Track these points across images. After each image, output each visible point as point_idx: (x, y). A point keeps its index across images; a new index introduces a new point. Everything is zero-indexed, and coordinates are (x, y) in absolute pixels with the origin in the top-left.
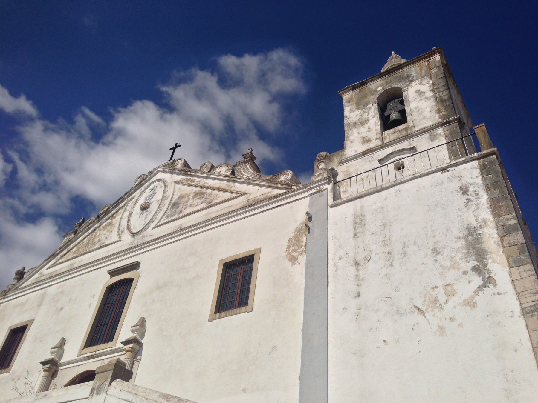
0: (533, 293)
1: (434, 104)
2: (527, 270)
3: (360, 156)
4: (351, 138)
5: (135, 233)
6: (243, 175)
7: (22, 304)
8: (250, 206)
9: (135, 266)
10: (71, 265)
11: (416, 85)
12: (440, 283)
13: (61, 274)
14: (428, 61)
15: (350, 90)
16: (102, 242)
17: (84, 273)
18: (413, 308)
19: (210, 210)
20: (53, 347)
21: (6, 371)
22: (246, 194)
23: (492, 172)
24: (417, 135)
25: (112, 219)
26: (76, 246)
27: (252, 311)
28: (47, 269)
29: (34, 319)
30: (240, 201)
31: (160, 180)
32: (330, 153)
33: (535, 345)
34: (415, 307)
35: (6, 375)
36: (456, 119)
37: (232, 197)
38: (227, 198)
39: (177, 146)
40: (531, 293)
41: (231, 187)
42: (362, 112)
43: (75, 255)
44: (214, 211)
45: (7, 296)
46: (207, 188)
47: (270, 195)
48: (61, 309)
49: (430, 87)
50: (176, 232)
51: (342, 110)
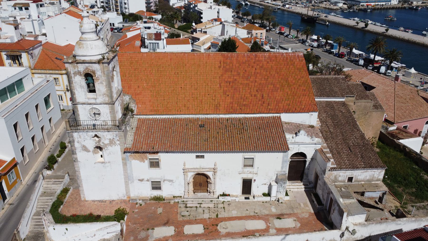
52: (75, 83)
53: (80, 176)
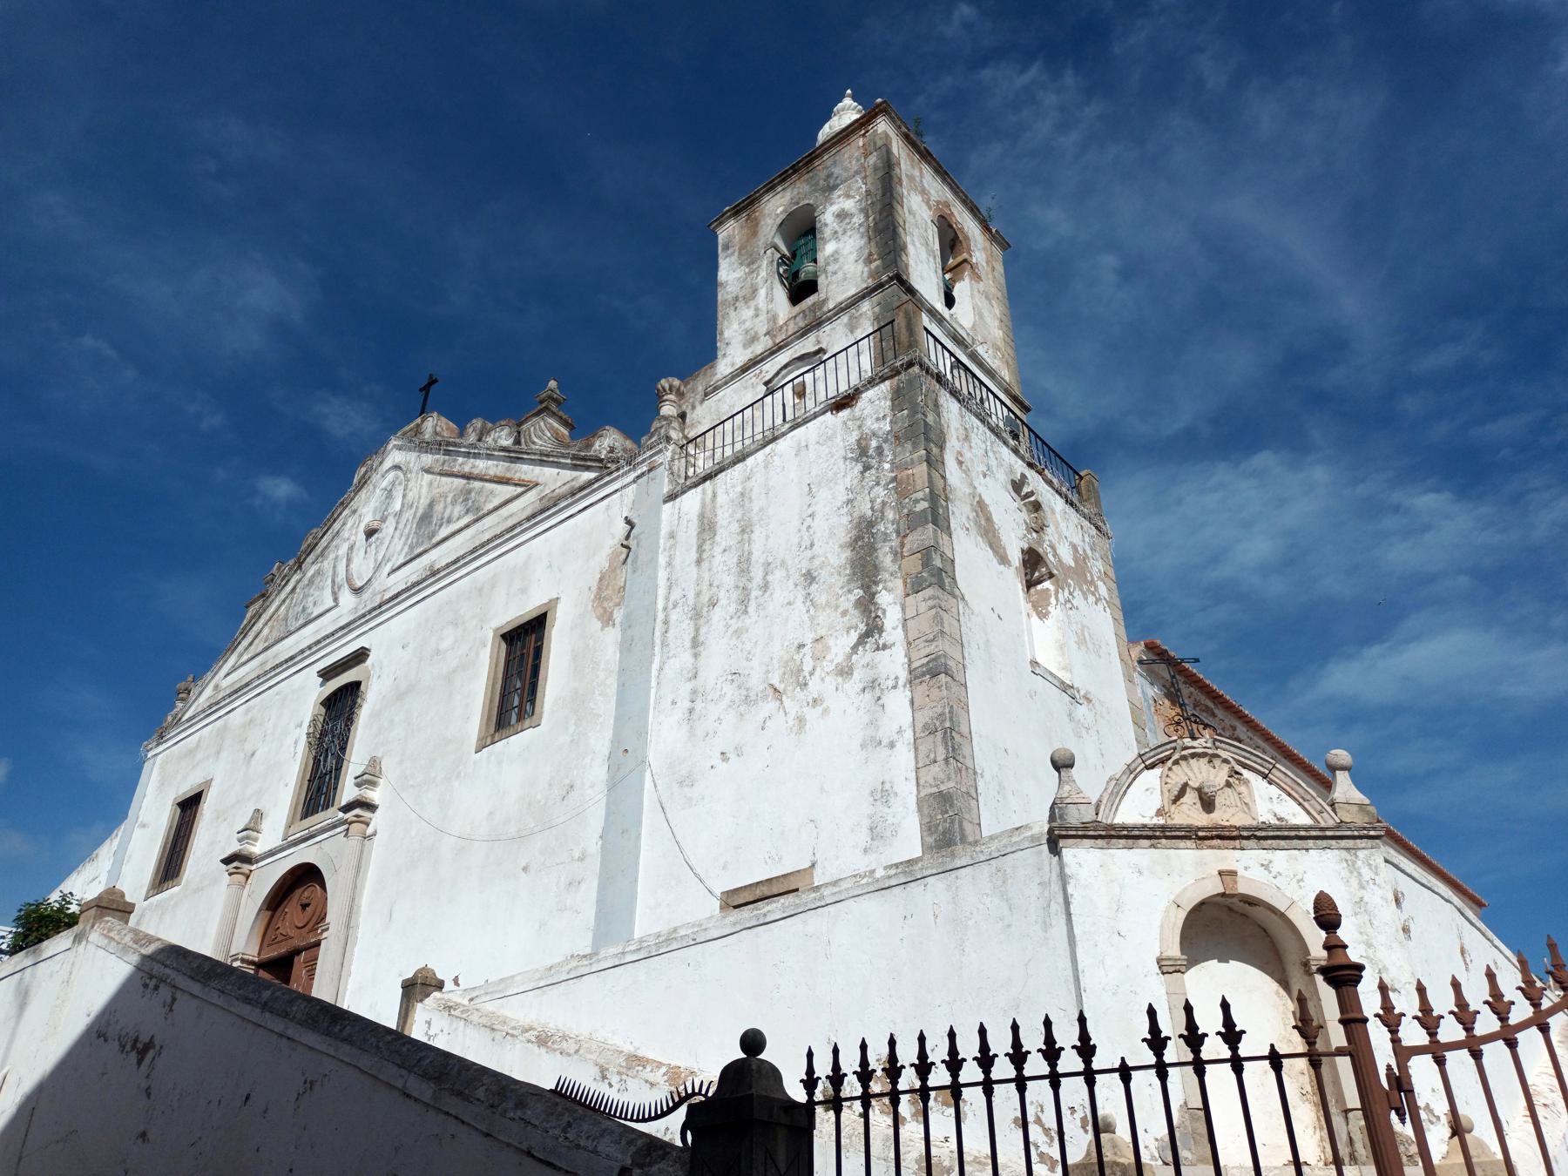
0: (929, 641)
1: (863, 242)
2: (927, 598)
3: (737, 375)
4: (727, 334)
5: (359, 589)
6: (534, 443)
7: (191, 752)
8: (542, 511)
9: (360, 656)
10: (261, 665)
11: (839, 197)
12: (808, 638)
13: (247, 685)
14: (864, 135)
15: (730, 217)
16: (309, 611)
17: (282, 680)
18: (768, 688)
19: (478, 525)
20: (240, 829)
21: (174, 884)
22: (537, 484)
23: (907, 405)
24: (830, 320)
25: (322, 562)
26: (266, 624)
27: (539, 725)
28: (228, 674)
29: (212, 779)
30: (530, 500)
31: (397, 467)
32: (681, 378)
33: (918, 735)
34: (771, 685)
35: (176, 889)
36: (891, 279)
37: (515, 493)
38: (508, 496)
39: (432, 382)
40: (926, 641)
41: (516, 472)
42: (747, 270)
43: (266, 645)
44: (490, 526)
45: (165, 739)
46: (475, 478)
47: (576, 484)
48: (253, 755)
49: (860, 201)
50: (424, 580)
51: (715, 267)
53: (964, 729)
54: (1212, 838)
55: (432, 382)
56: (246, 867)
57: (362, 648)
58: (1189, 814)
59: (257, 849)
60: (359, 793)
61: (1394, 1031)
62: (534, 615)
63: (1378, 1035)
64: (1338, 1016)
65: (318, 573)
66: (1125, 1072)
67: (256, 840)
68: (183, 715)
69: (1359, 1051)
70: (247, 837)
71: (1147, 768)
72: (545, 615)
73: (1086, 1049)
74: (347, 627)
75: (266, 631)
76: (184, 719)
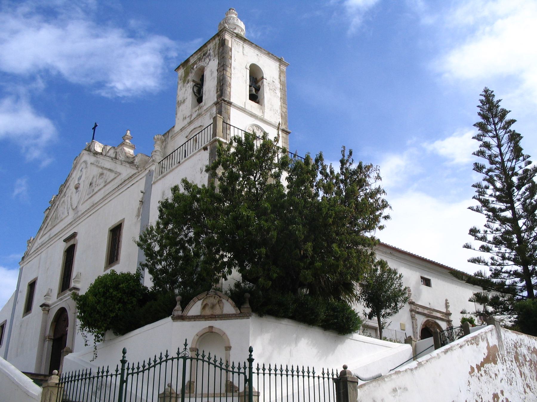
9: (74, 235)
39: (96, 126)
44: (110, 187)
52: (234, 69)
54: (209, 318)
55: (96, 126)
56: (47, 308)
57: (75, 232)
58: (208, 312)
59: (49, 302)
60: (45, 301)
61: (128, 371)
62: (119, 224)
63: (126, 371)
64: (121, 368)
65: (64, 201)
66: (319, 377)
67: (50, 299)
68: (30, 252)
69: (122, 374)
70: (47, 298)
71: (199, 300)
72: (121, 224)
73: (108, 372)
74: (71, 224)
75: (50, 223)
76: (29, 254)
